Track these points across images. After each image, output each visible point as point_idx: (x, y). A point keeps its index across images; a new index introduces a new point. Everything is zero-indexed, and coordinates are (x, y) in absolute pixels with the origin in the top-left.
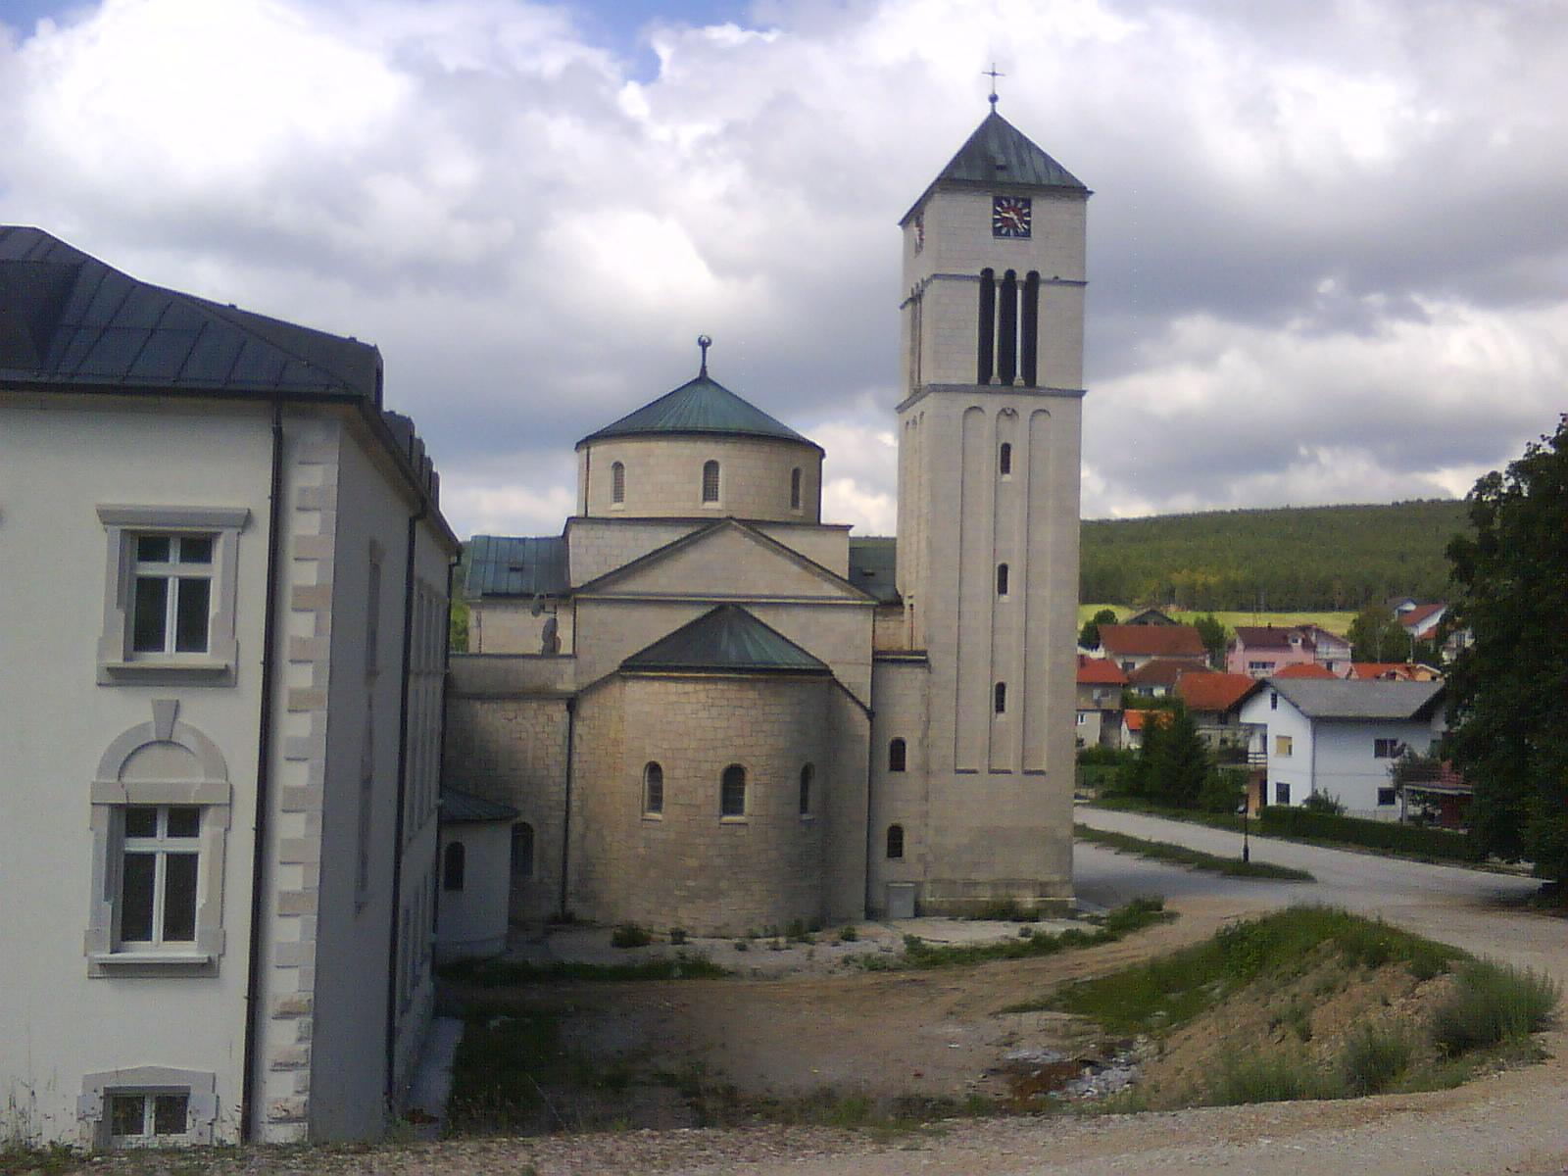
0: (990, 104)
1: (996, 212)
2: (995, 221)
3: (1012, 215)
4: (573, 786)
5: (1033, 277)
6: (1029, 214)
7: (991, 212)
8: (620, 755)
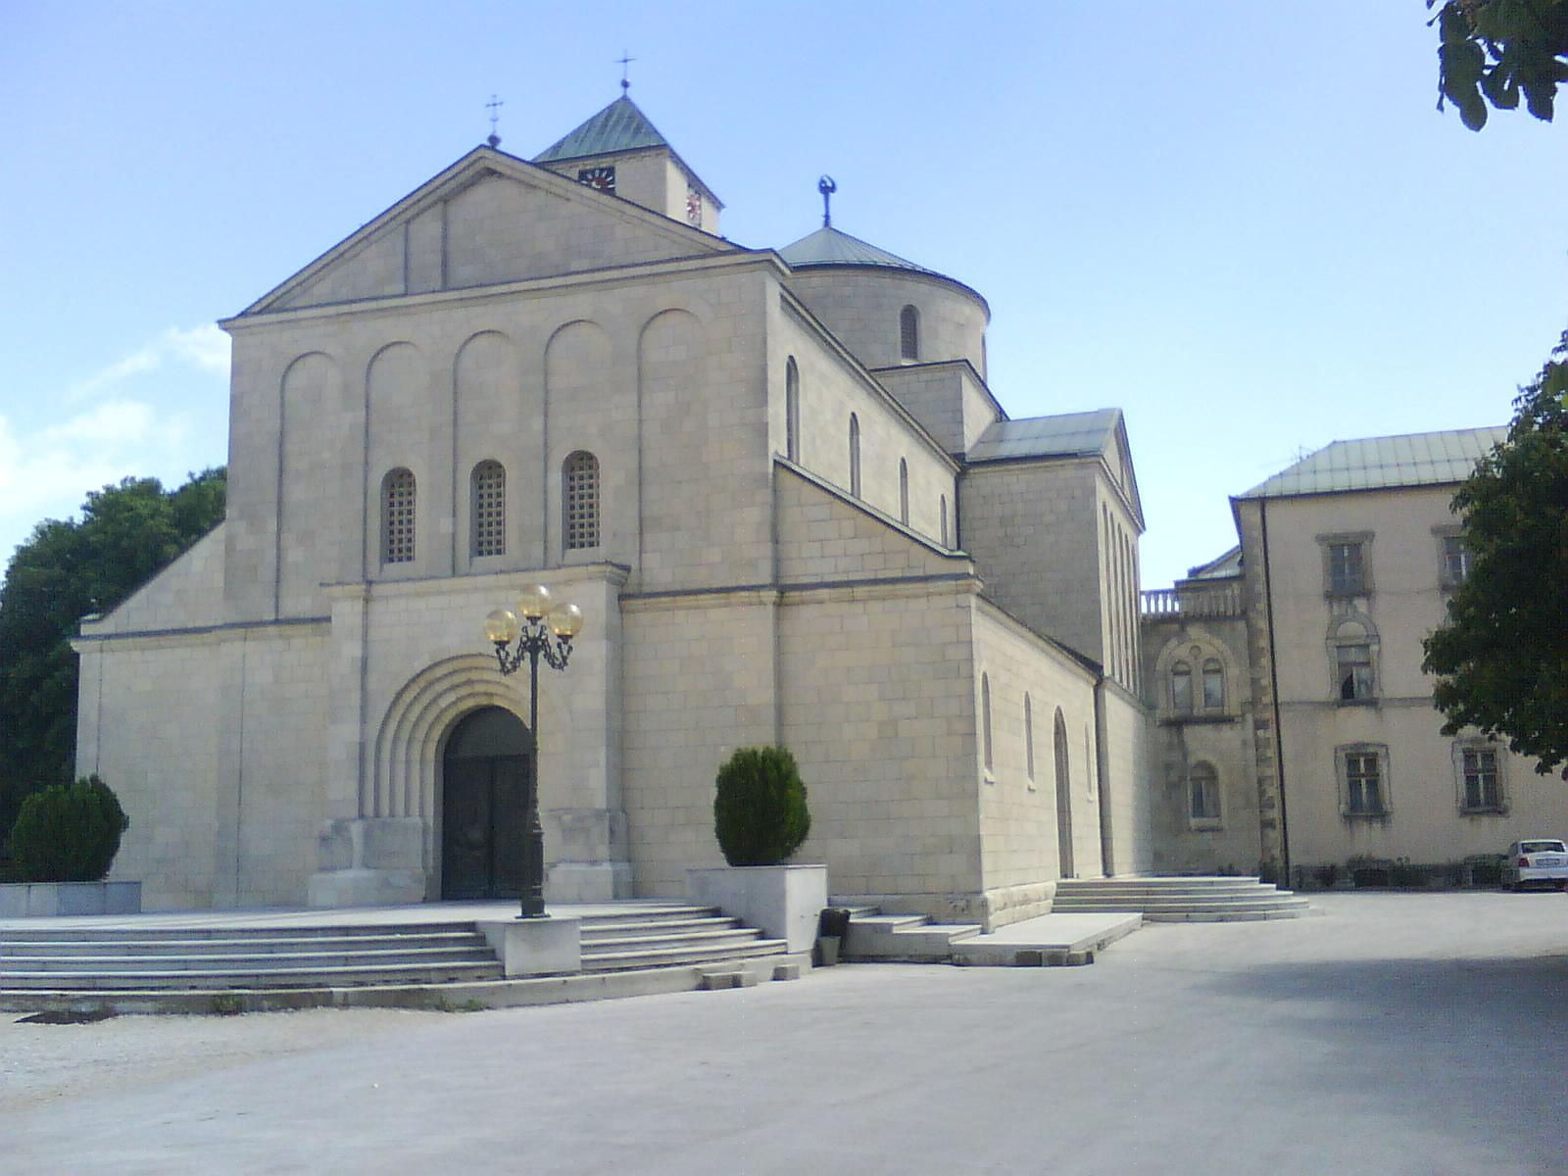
6: (612, 182)
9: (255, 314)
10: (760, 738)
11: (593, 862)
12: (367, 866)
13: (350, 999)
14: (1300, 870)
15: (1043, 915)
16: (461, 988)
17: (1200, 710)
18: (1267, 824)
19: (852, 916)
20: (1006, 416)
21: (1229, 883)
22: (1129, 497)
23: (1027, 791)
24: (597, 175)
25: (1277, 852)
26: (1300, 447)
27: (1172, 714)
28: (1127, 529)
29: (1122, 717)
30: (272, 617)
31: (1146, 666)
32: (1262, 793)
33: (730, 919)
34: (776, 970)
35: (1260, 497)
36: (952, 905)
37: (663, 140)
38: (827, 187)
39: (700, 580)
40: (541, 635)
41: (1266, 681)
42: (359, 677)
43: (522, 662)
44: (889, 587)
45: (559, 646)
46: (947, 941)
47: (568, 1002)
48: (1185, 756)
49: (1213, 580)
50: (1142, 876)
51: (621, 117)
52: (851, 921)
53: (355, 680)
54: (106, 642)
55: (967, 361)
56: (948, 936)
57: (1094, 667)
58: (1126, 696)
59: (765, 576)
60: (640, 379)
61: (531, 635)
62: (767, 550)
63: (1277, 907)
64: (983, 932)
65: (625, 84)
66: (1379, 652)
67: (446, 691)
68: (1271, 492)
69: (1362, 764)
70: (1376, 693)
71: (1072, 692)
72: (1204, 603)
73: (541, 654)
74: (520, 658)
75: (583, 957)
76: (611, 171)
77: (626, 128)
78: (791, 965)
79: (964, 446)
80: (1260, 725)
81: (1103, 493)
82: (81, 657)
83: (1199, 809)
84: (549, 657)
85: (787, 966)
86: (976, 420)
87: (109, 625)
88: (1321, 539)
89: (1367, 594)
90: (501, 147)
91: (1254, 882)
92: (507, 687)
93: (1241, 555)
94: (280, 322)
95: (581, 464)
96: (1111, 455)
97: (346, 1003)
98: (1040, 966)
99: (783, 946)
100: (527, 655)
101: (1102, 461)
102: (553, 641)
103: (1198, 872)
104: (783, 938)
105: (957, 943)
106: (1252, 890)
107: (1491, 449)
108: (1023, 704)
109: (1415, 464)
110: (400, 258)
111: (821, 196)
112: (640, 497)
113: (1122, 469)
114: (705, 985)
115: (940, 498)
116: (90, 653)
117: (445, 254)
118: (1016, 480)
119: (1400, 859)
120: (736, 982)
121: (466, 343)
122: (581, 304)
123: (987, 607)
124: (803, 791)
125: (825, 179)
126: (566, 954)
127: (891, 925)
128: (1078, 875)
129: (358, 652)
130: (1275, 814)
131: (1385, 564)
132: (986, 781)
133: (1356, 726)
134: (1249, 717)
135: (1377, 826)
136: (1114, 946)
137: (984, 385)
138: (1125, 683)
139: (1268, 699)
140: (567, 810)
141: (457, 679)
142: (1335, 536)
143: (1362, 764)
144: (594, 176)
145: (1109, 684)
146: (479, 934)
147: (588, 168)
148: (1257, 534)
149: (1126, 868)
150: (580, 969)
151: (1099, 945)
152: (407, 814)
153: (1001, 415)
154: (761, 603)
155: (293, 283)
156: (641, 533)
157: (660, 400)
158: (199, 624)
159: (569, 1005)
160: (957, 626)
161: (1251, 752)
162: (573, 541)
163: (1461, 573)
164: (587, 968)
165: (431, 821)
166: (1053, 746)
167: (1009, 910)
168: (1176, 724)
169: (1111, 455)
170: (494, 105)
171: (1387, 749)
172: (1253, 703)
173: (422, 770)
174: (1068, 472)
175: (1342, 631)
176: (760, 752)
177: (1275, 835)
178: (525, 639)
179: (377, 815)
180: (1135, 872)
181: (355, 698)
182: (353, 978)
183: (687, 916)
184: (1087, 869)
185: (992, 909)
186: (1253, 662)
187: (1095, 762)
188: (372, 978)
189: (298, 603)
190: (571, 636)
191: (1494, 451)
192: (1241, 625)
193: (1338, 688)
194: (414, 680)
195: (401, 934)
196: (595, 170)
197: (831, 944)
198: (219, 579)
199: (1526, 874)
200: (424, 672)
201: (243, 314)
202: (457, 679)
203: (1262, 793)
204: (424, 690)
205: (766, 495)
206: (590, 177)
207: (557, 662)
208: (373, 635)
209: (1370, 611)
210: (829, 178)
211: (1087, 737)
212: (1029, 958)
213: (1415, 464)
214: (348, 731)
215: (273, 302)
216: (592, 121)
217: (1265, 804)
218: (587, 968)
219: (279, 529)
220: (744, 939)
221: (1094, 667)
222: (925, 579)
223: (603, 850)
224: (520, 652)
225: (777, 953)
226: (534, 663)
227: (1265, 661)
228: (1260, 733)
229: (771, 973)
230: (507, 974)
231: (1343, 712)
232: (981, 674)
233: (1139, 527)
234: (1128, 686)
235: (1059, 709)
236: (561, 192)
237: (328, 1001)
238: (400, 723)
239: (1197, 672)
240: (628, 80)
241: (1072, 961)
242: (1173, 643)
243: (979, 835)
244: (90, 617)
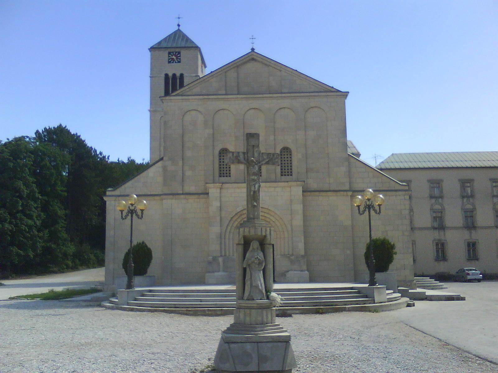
0: (178, 27)
1: (169, 57)
2: (169, 59)
3: (174, 57)
4: (394, 189)
5: (182, 76)
6: (180, 56)
7: (168, 57)
8: (326, 359)
12: (224, 271)
24: (174, 54)
39: (326, 187)
54: (117, 198)
61: (368, 204)
69: (440, 245)
74: (365, 211)
76: (179, 53)
82: (107, 202)
87: (117, 192)
90: (255, 51)
94: (182, 99)
98: (454, 300)
116: (110, 201)
117: (238, 83)
121: (248, 111)
122: (286, 103)
129: (219, 205)
143: (440, 245)
144: (173, 54)
147: (171, 51)
154: (347, 195)
170: (252, 39)
171: (415, 242)
182: (343, 303)
190: (360, 205)
194: (236, 214)
195: (339, 290)
196: (174, 52)
198: (160, 179)
199: (469, 277)
206: (172, 54)
214: (216, 230)
216: (170, 36)
222: (396, 191)
236: (279, 68)
240: (180, 24)
244: (110, 189)
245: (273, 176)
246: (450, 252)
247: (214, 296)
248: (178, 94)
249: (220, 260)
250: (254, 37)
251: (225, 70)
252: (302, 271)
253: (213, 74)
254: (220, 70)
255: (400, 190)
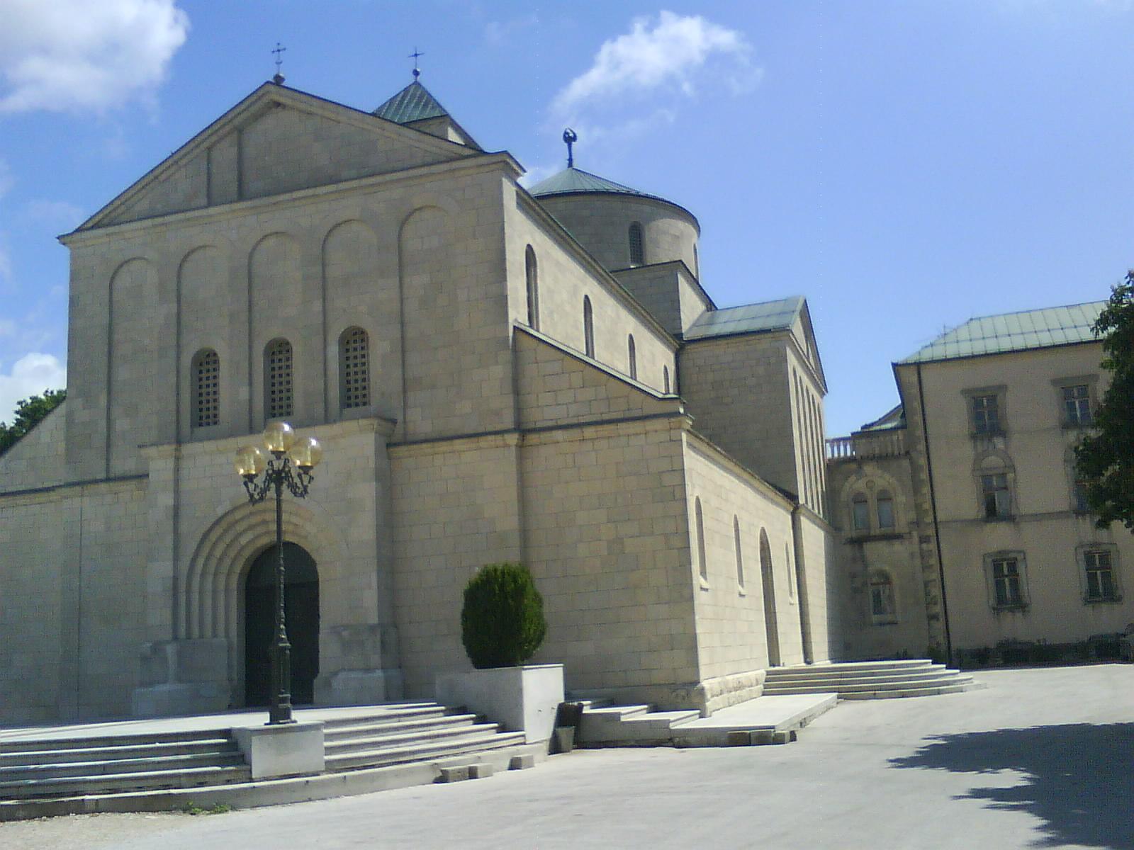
9: (88, 229)
10: (509, 557)
11: (368, 670)
12: (180, 680)
13: (88, 807)
14: (959, 651)
15: (755, 698)
16: (209, 792)
17: (876, 531)
18: (934, 617)
19: (585, 708)
20: (715, 307)
21: (907, 665)
22: (813, 365)
23: (738, 596)
25: (941, 639)
26: (945, 327)
27: (854, 534)
28: (813, 391)
29: (815, 538)
30: (102, 475)
31: (831, 499)
32: (927, 594)
33: (474, 716)
34: (512, 761)
35: (915, 363)
36: (674, 694)
37: (444, 110)
38: (569, 137)
40: (284, 467)
41: (927, 506)
42: (171, 522)
43: (267, 492)
44: (612, 427)
45: (299, 475)
46: (668, 728)
47: (310, 800)
48: (866, 566)
49: (880, 430)
50: (835, 663)
51: (413, 96)
52: (584, 712)
53: (169, 525)
55: (681, 261)
56: (669, 721)
57: (791, 497)
58: (817, 521)
59: (508, 421)
60: (401, 265)
62: (509, 401)
63: (948, 683)
64: (702, 716)
65: (416, 73)
66: (1015, 480)
67: (245, 531)
68: (926, 356)
70: (1014, 512)
71: (776, 519)
72: (876, 447)
73: (284, 486)
74: (266, 489)
75: (327, 758)
77: (417, 104)
78: (526, 755)
79: (681, 328)
80: (924, 539)
81: (792, 360)
83: (878, 609)
84: (293, 487)
85: (521, 756)
86: (690, 309)
88: (965, 392)
89: (1003, 434)
90: (284, 84)
91: (927, 664)
92: (296, 525)
93: (903, 412)
95: (354, 340)
96: (798, 330)
97: (97, 809)
99: (522, 738)
100: (273, 485)
101: (791, 335)
102: (294, 473)
103: (880, 657)
104: (521, 731)
105: (676, 728)
106: (925, 671)
107: (1126, 278)
108: (733, 524)
109: (1036, 332)
110: (204, 178)
111: (566, 145)
112: (404, 362)
113: (807, 346)
114: (443, 779)
115: (663, 368)
118: (720, 348)
119: (1039, 641)
120: (472, 774)
123: (697, 443)
124: (538, 600)
125: (569, 131)
126: (312, 755)
127: (619, 714)
128: (783, 664)
130: (938, 609)
131: (1016, 409)
132: (702, 589)
133: (999, 537)
134: (915, 534)
135: (1019, 615)
136: (814, 723)
137: (698, 283)
138: (816, 511)
139: (930, 519)
140: (346, 627)
141: (254, 520)
142: (977, 390)
145: (802, 510)
146: (233, 741)
148: (915, 391)
149: (826, 655)
150: (323, 769)
151: (801, 723)
152: (215, 635)
153: (710, 306)
154: (506, 446)
155: (118, 202)
156: (405, 392)
157: (417, 282)
158: (47, 485)
159: (311, 803)
160: (671, 457)
161: (918, 562)
162: (349, 402)
163: (1077, 414)
164: (331, 767)
165: (235, 640)
166: (759, 560)
167: (725, 695)
168: (858, 542)
169: (798, 330)
171: (1024, 554)
172: (917, 523)
173: (227, 597)
174: (765, 343)
175: (985, 464)
176: (500, 568)
177: (939, 625)
178: (270, 472)
179: (189, 636)
180: (830, 659)
181: (169, 539)
182: (101, 786)
183: (434, 715)
184: (792, 659)
185: (709, 696)
186: (916, 491)
187: (796, 581)
188: (124, 785)
189: (123, 464)
190: (311, 468)
191: (1128, 279)
192: (905, 463)
193: (984, 508)
197: (567, 734)
200: (226, 514)
201: (79, 230)
202: (254, 520)
203: (927, 594)
204: (226, 531)
205: (506, 356)
207: (299, 491)
208: (184, 486)
209: (1006, 447)
210: (571, 131)
211: (787, 553)
212: (740, 738)
213: (1036, 332)
214: (162, 568)
215: (103, 218)
217: (931, 602)
218: (331, 767)
219: (109, 402)
220: (487, 733)
221: (791, 497)
223: (376, 659)
224: (267, 484)
225: (515, 745)
226: (279, 492)
227: (926, 490)
228: (924, 546)
229: (507, 764)
230: (253, 777)
231: (989, 526)
232: (695, 498)
233: (822, 389)
234: (819, 513)
235: (763, 530)
237: (81, 809)
238: (208, 559)
239: (872, 502)
241: (778, 740)
242: (853, 478)
243: (695, 634)
245: (319, 410)
246: (1034, 580)
247: (84, 757)
248: (99, 221)
249: (170, 650)
250: (281, 47)
251: (206, 145)
252: (368, 670)
253: (175, 158)
254: (192, 145)
255: (655, 416)
